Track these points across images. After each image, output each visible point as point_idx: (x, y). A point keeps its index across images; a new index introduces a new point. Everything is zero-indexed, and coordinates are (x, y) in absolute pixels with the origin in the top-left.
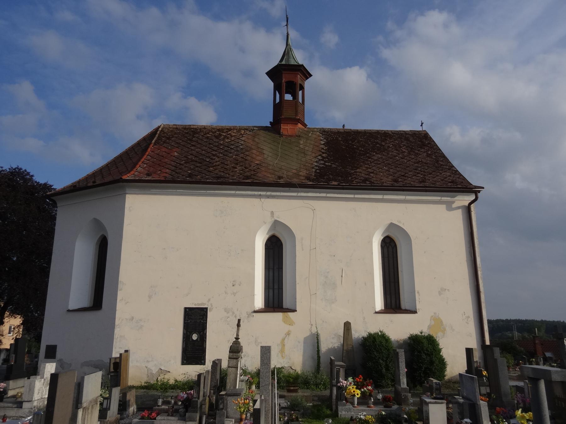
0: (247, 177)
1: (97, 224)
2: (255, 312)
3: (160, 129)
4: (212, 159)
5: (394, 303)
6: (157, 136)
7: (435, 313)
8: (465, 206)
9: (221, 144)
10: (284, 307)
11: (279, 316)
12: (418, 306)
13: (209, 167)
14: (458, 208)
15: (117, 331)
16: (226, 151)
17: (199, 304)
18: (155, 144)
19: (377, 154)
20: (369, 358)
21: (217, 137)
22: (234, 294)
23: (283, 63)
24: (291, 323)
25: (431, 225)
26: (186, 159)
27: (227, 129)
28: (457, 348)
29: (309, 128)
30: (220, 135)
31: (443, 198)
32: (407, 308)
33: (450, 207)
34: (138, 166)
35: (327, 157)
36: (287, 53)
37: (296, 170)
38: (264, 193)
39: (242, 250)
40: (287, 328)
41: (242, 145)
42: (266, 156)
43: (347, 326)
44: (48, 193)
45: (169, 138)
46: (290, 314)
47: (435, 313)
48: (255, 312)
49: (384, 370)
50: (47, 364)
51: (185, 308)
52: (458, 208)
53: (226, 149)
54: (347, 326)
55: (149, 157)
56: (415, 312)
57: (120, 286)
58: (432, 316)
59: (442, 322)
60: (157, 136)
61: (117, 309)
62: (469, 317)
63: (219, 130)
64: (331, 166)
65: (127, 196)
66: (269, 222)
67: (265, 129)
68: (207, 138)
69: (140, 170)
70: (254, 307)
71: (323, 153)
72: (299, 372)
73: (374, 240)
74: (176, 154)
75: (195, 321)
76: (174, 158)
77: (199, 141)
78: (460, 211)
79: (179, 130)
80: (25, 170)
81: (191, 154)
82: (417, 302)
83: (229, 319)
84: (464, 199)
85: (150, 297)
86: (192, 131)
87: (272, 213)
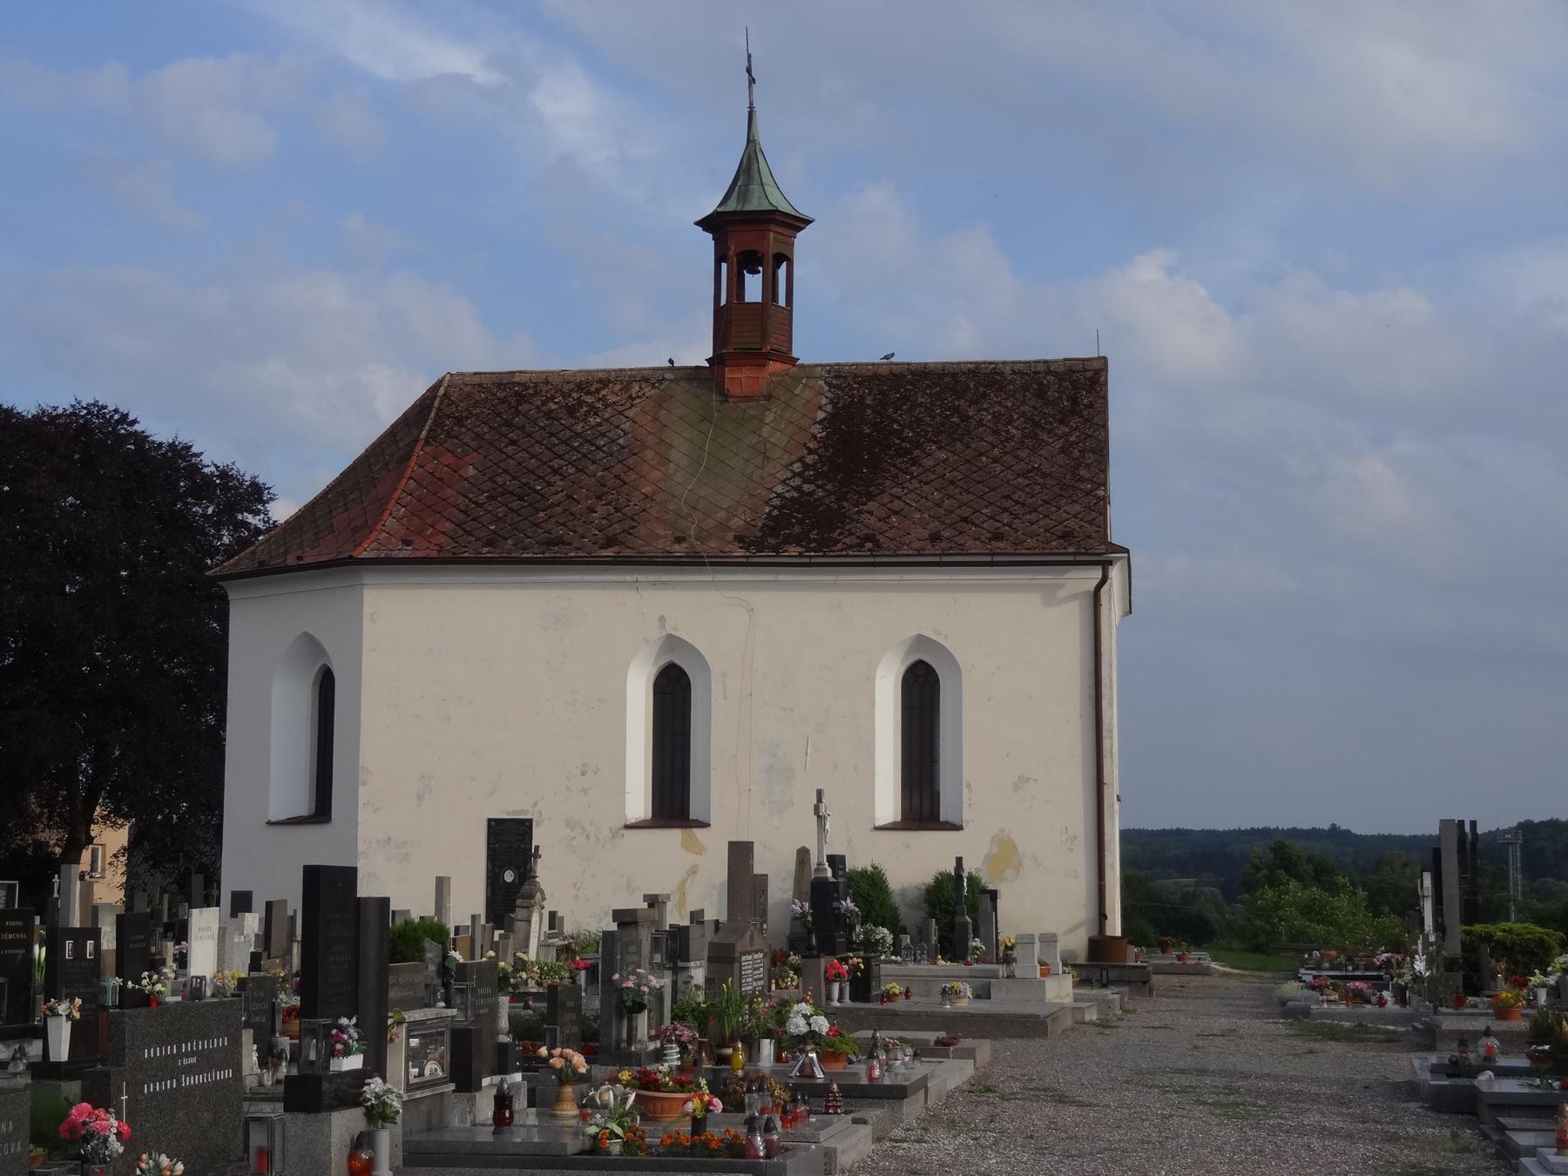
0: (610, 542)
1: (310, 643)
2: (628, 827)
3: (442, 391)
4: (549, 484)
5: (923, 806)
6: (170, 1084)
7: (1002, 830)
9: (578, 435)
11: (674, 836)
12: (967, 815)
13: (538, 511)
14: (1074, 597)
16: (585, 456)
17: (515, 812)
18: (427, 442)
19: (939, 448)
20: (838, 914)
21: (571, 411)
22: (585, 791)
23: (732, 206)
24: (698, 850)
25: (1006, 634)
26: (490, 485)
27: (600, 381)
28: (1051, 897)
29: (802, 366)
30: (580, 402)
32: (950, 819)
34: (387, 513)
36: (749, 169)
37: (727, 510)
38: (642, 578)
40: (690, 859)
41: (626, 433)
42: (672, 466)
45: (459, 421)
46: (697, 832)
47: (1002, 830)
48: (628, 827)
51: (490, 820)
52: (1074, 597)
53: (586, 448)
54: (959, 860)
55: (412, 484)
56: (958, 828)
57: (362, 776)
59: (1014, 847)
60: (170, 1084)
61: (628, 789)
62: (1075, 837)
63: (580, 387)
64: (812, 493)
65: (366, 592)
66: (657, 634)
68: (548, 414)
71: (811, 451)
73: (880, 673)
74: (471, 471)
75: (510, 845)
76: (466, 484)
77: (529, 429)
79: (488, 390)
80: (116, 411)
81: (506, 471)
82: (965, 806)
83: (574, 843)
85: (420, 798)
86: (517, 394)
87: (662, 619)
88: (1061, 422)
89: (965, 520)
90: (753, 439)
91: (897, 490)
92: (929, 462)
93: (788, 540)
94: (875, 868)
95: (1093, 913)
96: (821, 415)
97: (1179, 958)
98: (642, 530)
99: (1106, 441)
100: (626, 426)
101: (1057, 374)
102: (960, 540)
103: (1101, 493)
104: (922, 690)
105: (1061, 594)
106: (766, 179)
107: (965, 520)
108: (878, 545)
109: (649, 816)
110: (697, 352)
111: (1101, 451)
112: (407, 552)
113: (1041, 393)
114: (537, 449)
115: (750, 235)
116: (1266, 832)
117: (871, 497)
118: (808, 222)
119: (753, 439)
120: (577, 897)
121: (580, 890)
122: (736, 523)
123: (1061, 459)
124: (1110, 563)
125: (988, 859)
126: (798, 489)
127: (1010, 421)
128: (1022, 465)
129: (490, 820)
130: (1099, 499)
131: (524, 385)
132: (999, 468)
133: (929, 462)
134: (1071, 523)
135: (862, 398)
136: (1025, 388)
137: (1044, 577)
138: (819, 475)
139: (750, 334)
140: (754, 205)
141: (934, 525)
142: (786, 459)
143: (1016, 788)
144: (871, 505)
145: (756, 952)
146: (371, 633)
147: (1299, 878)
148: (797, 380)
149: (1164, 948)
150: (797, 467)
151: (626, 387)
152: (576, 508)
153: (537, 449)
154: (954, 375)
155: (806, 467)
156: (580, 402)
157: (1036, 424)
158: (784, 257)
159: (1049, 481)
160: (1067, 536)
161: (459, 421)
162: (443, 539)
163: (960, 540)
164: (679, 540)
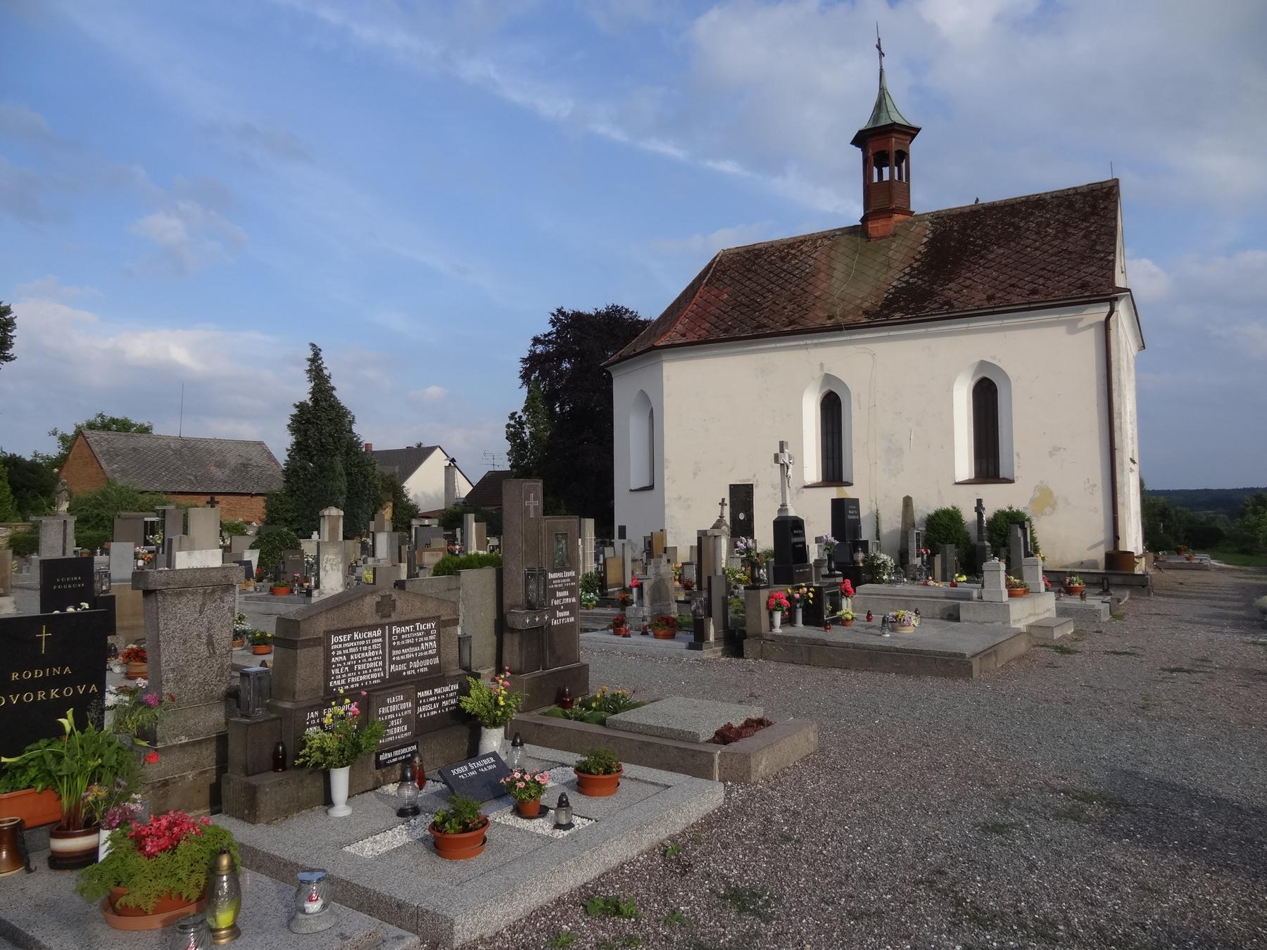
0: (791, 323)
5: (989, 465)
10: (1001, 476)
12: (1017, 473)
14: (1091, 326)
15: (667, 510)
21: (782, 259)
25: (1042, 355)
30: (788, 254)
33: (1073, 328)
35: (917, 268)
38: (809, 342)
43: (907, 502)
44: (127, 698)
45: (724, 273)
54: (907, 502)
56: (1012, 482)
59: (1051, 493)
66: (819, 374)
67: (852, 230)
68: (770, 263)
69: (673, 336)
71: (917, 260)
73: (956, 387)
74: (726, 296)
78: (1092, 331)
84: (1098, 313)
85: (695, 474)
87: (822, 365)
88: (1084, 220)
89: (1012, 285)
90: (882, 259)
91: (969, 275)
92: (991, 256)
93: (895, 311)
95: (1110, 535)
96: (925, 240)
98: (811, 315)
99: (1115, 227)
100: (811, 262)
101: (1082, 194)
102: (1008, 297)
103: (1111, 258)
104: (986, 397)
105: (1081, 325)
106: (890, 108)
107: (1012, 285)
108: (952, 306)
110: (853, 212)
111: (1112, 234)
112: (683, 340)
113: (1071, 206)
114: (762, 280)
115: (883, 143)
116: (1252, 490)
117: (951, 280)
118: (918, 130)
119: (882, 259)
122: (866, 305)
123: (1083, 242)
124: (1116, 299)
125: (1032, 501)
126: (907, 282)
127: (1048, 225)
128: (1055, 250)
130: (1109, 261)
131: (760, 250)
132: (1038, 253)
133: (991, 256)
134: (1088, 279)
135: (952, 227)
136: (1060, 205)
137: (1068, 315)
138: (920, 272)
139: (883, 199)
140: (884, 122)
141: (989, 292)
142: (902, 266)
143: (1051, 454)
144: (950, 285)
145: (423, 620)
146: (668, 386)
148: (912, 223)
149: (1179, 552)
150: (907, 270)
151: (815, 242)
152: (776, 308)
153: (762, 280)
154: (1012, 206)
155: (913, 269)
156: (788, 254)
157: (1067, 225)
158: (903, 156)
159: (1073, 256)
160: (1084, 286)
161: (724, 273)
162: (703, 332)
163: (1008, 297)
164: (830, 318)
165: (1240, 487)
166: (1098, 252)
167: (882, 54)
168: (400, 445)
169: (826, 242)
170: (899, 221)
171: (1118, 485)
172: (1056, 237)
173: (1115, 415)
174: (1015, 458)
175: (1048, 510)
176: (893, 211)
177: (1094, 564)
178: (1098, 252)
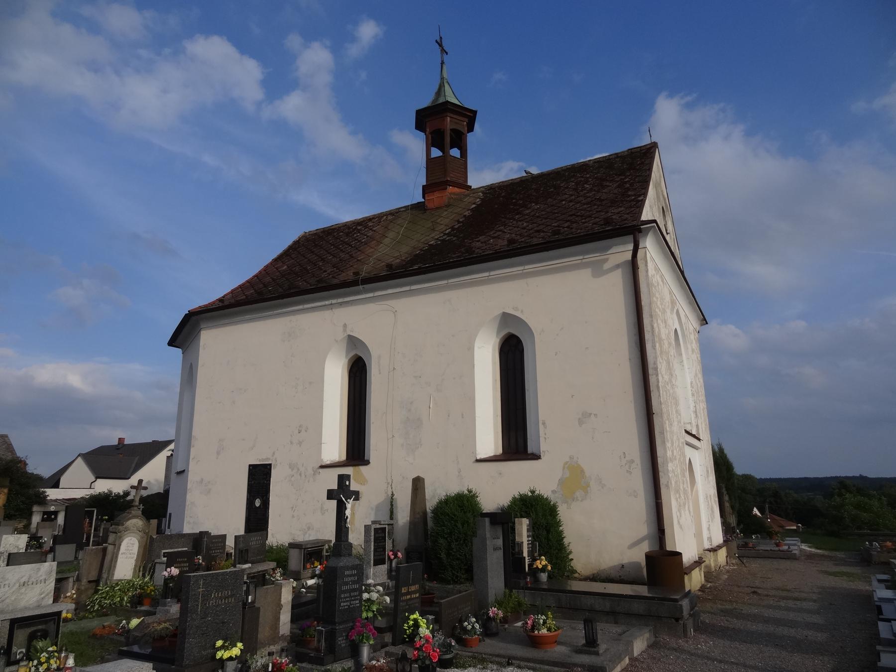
2: (322, 467)
5: (517, 442)
8: (628, 261)
10: (530, 450)
12: (544, 447)
14: (618, 266)
15: (188, 497)
17: (263, 460)
25: (565, 302)
31: (450, 281)
33: (598, 271)
36: (440, 91)
38: (334, 301)
39: (310, 383)
43: (418, 484)
47: (571, 458)
48: (322, 467)
49: (443, 556)
50: (4, 536)
54: (418, 484)
58: (566, 463)
59: (582, 471)
62: (632, 461)
66: (341, 336)
70: (322, 460)
72: (713, 570)
73: (477, 344)
82: (542, 440)
83: (293, 479)
84: (621, 252)
85: (218, 453)
87: (345, 326)
94: (470, 491)
97: (778, 545)
105: (606, 266)
109: (344, 457)
116: (836, 477)
120: (293, 517)
121: (302, 515)
125: (562, 482)
128: (589, 199)
129: (250, 466)
132: (571, 204)
139: (442, 175)
143: (581, 422)
147: (850, 492)
165: (829, 476)
166: (629, 196)
167: (444, 51)
168: (148, 439)
169: (390, 217)
170: (454, 194)
171: (660, 460)
172: (591, 190)
173: (651, 371)
174: (541, 427)
175: (579, 494)
176: (447, 183)
177: (637, 565)
178: (629, 196)
